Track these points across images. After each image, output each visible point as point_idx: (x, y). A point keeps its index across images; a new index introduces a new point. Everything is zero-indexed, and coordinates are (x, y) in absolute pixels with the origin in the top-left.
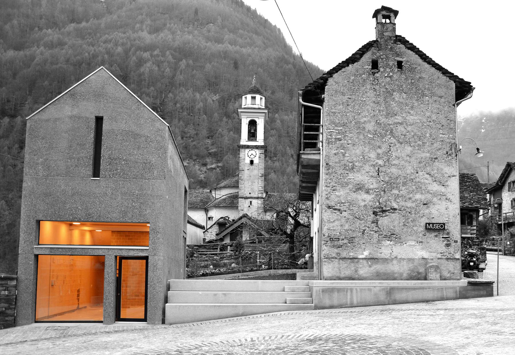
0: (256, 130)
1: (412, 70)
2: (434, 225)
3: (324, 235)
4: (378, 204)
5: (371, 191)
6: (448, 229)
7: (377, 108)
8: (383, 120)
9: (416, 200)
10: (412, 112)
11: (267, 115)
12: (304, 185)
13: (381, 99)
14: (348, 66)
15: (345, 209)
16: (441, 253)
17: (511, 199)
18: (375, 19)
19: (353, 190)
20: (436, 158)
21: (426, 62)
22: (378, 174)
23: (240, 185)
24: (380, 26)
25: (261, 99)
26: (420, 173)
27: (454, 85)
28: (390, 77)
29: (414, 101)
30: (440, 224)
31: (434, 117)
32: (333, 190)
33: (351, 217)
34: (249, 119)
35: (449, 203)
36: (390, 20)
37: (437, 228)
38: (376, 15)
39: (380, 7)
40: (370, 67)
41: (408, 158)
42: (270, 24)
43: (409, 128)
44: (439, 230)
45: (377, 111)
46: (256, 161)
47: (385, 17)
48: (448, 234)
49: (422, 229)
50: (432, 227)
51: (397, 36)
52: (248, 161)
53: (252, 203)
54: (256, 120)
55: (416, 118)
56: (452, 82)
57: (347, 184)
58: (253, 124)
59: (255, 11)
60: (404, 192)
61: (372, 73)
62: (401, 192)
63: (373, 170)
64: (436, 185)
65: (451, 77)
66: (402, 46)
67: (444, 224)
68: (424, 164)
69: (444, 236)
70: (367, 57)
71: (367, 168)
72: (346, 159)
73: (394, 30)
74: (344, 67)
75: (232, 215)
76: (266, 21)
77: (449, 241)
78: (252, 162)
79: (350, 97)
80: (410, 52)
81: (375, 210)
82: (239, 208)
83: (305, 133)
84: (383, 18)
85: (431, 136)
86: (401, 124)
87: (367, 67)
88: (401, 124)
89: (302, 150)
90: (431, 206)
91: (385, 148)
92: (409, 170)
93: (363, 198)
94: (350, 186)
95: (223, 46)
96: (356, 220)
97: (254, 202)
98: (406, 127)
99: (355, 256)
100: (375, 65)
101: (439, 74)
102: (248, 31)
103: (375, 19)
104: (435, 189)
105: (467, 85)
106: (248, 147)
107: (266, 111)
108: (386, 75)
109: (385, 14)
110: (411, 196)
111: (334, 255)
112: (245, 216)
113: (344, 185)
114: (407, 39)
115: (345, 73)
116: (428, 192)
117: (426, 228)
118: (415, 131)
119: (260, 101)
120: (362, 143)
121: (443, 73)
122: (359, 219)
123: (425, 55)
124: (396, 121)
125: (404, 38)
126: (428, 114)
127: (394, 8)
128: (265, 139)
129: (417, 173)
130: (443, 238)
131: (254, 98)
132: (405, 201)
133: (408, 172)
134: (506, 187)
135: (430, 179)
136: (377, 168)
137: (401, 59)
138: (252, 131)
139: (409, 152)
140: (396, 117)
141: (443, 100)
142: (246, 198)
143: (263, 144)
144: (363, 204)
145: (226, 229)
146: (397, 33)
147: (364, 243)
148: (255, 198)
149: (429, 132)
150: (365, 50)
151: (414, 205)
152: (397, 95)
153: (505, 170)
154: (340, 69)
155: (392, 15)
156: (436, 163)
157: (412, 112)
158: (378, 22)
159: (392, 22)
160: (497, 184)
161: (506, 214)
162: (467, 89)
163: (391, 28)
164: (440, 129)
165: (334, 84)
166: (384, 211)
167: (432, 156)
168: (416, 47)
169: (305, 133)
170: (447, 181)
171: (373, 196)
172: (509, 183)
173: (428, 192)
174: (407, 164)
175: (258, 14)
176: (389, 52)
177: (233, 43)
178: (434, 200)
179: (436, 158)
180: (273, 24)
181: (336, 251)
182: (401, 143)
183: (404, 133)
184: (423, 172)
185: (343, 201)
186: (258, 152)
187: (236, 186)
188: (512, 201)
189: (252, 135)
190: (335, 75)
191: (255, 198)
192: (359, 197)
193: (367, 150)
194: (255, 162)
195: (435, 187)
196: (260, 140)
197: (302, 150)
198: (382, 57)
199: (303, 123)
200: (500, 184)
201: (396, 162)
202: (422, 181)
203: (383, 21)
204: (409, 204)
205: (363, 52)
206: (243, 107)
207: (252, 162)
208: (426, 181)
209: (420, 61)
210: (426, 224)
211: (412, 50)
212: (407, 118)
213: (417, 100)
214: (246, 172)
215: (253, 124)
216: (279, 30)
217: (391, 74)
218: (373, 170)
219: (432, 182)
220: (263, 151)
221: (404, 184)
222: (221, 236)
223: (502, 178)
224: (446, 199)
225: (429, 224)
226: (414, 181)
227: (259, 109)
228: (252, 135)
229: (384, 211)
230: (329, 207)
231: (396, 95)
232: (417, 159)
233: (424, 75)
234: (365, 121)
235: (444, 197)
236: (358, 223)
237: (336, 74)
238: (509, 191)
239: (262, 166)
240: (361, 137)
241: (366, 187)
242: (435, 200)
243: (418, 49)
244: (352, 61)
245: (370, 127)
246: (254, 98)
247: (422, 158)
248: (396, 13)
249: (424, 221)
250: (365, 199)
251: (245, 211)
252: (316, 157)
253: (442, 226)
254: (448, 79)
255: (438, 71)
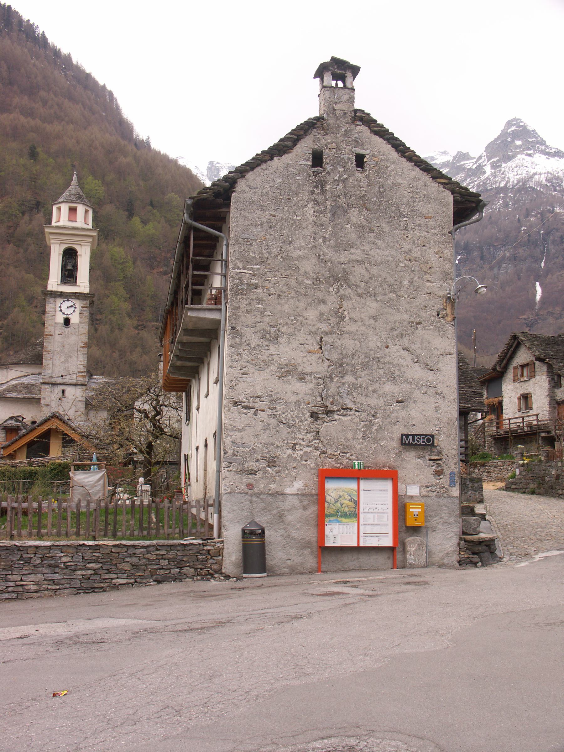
0: (75, 267)
1: (380, 170)
2: (416, 438)
3: (226, 453)
4: (319, 399)
5: (308, 378)
6: (438, 445)
7: (321, 234)
8: (330, 254)
9: (385, 395)
10: (379, 243)
11: (96, 241)
12: (179, 363)
13: (325, 219)
14: (272, 159)
15: (262, 408)
16: (427, 487)
17: (519, 395)
18: (318, 79)
19: (278, 374)
20: (420, 323)
21: (405, 157)
22: (321, 348)
23: (44, 361)
24: (327, 93)
25: (86, 212)
26: (393, 348)
27: (450, 198)
28: (345, 181)
29: (384, 225)
30: (426, 435)
31: (416, 253)
32: (243, 374)
33: (273, 422)
34: (64, 247)
35: (440, 401)
36: (344, 82)
37: (421, 442)
38: (320, 73)
39: (328, 60)
40: (310, 163)
41: (372, 321)
42: (95, 83)
43: (374, 271)
44: (423, 446)
45: (321, 240)
46: (75, 319)
47: (336, 77)
48: (440, 453)
49: (395, 444)
50: (411, 441)
51: (356, 111)
52: (60, 319)
53: (66, 393)
54: (77, 248)
55: (386, 253)
56: (448, 193)
57: (267, 364)
58: (70, 255)
59: (68, 58)
60: (363, 380)
61: (314, 172)
62: (360, 380)
63: (311, 341)
64: (419, 369)
65: (446, 184)
66: (363, 128)
67: (433, 436)
68: (400, 333)
69: (433, 458)
70: (305, 147)
71: (302, 337)
72: (266, 319)
73: (351, 100)
74: (266, 162)
75: (29, 415)
76: (88, 76)
77: (439, 465)
78: (67, 322)
79: (273, 213)
80: (377, 140)
81: (315, 409)
82: (42, 401)
83: (195, 273)
84: (333, 80)
85: (411, 283)
86: (361, 262)
87: (304, 163)
88: (361, 262)
89: (189, 302)
90: (412, 405)
91: (332, 301)
92: (374, 342)
93: (294, 388)
94: (273, 368)
95: (11, 116)
96: (282, 426)
97: (70, 391)
98: (369, 268)
99: (279, 489)
100: (317, 159)
101: (426, 178)
102: (56, 94)
103: (318, 79)
104: (417, 376)
105: (473, 199)
106: (61, 295)
107: (95, 234)
108: (336, 178)
109: (338, 71)
110: (376, 386)
111: (243, 487)
112: (54, 416)
113: (263, 365)
114: (374, 116)
115: (266, 172)
116: (406, 381)
117: (402, 444)
118: (384, 275)
119: (84, 218)
120: (293, 294)
121: (434, 178)
122: (287, 425)
123: (403, 145)
124: (352, 257)
125: (369, 115)
126: (407, 247)
127: (353, 62)
128: (92, 281)
129: (387, 347)
130: (430, 460)
131: (73, 210)
132: (366, 395)
133: (372, 345)
134: (510, 375)
135: (409, 357)
136: (318, 339)
137: (362, 152)
138: (69, 267)
139: (373, 312)
140: (353, 250)
141: (432, 223)
142: (54, 384)
143: (87, 290)
144: (294, 398)
145: (20, 438)
146: (357, 106)
147: (294, 468)
148: (71, 385)
149: (408, 278)
150: (302, 133)
151: (381, 402)
152: (355, 214)
153: (510, 346)
154: (259, 165)
155: (349, 74)
156: (420, 331)
157: (379, 243)
158: (325, 84)
159: (349, 86)
160: (494, 369)
161: (509, 420)
162: (474, 205)
163: (346, 97)
164: (426, 272)
165: (247, 189)
166: (328, 412)
167: (412, 319)
168: (388, 130)
169: (195, 273)
170: (437, 362)
171: (311, 386)
172: (514, 368)
173: (406, 381)
174: (370, 332)
175: (75, 63)
176: (341, 138)
177: (29, 113)
178: (414, 395)
179: (420, 323)
180: (101, 83)
181: (246, 479)
182: (360, 296)
183: (366, 278)
184: (397, 347)
185: (260, 394)
186: (78, 304)
187: (37, 360)
188: (519, 399)
189: (69, 275)
190: (250, 176)
191: (71, 385)
192: (288, 387)
193: (302, 305)
194: (72, 321)
195: (417, 372)
196: (83, 283)
197: (189, 302)
198: (329, 146)
199: (191, 256)
200: (498, 369)
201: (352, 328)
202: (396, 361)
203: (333, 83)
204: (373, 401)
205: (298, 136)
206: (53, 224)
207: (67, 322)
208: (402, 362)
209: (394, 155)
210: (402, 435)
211: (381, 137)
212: (372, 253)
213: (388, 222)
214: (57, 338)
215: (70, 255)
216: (111, 93)
217: (345, 176)
218: (311, 341)
219: (410, 363)
220: (86, 303)
221: (365, 366)
222: (10, 451)
223: (503, 359)
224: (437, 393)
225: (407, 436)
226: (382, 360)
227: (82, 229)
228: (69, 275)
229: (328, 412)
230: (235, 404)
231: (354, 214)
232: (387, 324)
233: (400, 181)
234: (300, 256)
235: (432, 391)
236: (285, 433)
237: (251, 173)
238: (514, 381)
239: (85, 328)
240: (293, 283)
241: (300, 369)
242: (417, 394)
243: (393, 134)
244: (279, 151)
245: (308, 266)
246: (73, 210)
247: (395, 322)
248: (355, 70)
249: (401, 430)
250: (299, 391)
251: (55, 408)
252: (214, 316)
253: (428, 440)
254: (441, 188)
255: (425, 174)
